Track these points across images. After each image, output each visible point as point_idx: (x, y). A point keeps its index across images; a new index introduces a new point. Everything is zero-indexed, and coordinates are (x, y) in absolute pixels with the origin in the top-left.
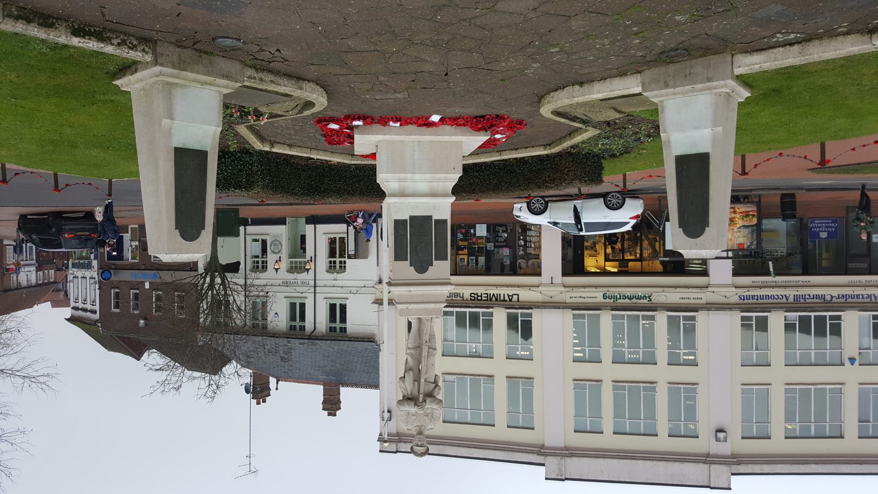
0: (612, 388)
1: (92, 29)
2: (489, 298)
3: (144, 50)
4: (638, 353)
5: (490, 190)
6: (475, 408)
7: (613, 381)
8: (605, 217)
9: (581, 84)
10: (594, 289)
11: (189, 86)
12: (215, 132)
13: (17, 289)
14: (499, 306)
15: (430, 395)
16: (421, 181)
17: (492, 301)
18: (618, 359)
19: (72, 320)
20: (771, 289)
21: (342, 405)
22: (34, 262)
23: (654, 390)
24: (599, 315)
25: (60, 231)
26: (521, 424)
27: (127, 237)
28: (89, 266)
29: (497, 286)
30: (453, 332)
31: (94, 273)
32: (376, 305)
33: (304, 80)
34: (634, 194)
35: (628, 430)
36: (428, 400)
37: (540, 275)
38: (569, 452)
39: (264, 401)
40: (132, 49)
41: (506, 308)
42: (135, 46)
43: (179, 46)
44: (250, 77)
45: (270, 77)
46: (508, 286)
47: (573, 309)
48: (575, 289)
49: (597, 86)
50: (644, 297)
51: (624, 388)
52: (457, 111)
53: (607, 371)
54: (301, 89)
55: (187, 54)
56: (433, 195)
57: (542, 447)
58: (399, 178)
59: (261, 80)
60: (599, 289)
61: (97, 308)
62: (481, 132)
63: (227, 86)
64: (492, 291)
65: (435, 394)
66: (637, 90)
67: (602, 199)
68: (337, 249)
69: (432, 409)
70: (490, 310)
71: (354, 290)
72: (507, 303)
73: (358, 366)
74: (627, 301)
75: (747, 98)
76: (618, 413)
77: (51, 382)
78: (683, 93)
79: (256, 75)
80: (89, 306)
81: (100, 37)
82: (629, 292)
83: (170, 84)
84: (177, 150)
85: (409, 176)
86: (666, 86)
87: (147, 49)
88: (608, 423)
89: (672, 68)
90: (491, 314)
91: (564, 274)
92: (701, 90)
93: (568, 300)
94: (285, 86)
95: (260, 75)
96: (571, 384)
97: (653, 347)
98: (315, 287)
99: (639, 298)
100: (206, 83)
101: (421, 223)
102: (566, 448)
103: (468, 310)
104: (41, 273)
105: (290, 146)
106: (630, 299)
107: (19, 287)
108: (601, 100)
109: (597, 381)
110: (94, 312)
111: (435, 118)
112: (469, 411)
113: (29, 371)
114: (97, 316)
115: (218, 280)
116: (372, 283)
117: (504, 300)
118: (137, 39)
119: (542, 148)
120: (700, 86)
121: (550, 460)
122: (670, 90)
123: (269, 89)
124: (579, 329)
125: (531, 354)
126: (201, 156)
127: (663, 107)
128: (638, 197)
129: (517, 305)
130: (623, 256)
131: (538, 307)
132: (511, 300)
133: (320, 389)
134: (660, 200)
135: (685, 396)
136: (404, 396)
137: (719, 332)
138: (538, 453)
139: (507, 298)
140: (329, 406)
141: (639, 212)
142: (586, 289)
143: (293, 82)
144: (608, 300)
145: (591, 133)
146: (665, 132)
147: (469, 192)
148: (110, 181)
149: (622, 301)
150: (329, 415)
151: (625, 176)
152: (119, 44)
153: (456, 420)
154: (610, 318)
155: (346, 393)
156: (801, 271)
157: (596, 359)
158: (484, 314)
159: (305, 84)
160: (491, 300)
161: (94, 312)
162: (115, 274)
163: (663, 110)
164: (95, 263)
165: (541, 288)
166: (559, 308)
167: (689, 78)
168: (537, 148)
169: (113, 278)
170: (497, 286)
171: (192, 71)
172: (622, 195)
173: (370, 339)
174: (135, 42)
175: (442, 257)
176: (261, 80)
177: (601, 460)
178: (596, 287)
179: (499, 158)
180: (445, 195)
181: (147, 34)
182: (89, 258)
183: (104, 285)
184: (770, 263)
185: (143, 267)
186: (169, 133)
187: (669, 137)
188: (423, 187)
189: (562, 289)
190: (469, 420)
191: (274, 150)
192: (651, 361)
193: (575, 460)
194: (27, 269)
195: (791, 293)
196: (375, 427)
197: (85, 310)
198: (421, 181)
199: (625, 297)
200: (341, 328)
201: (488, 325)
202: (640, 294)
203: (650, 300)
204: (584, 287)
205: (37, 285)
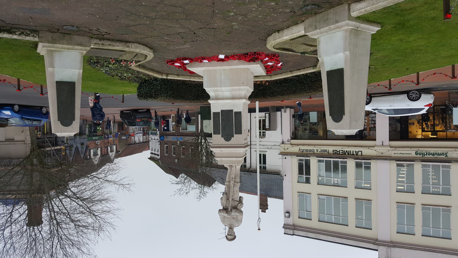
0: (421, 209)
1: (5, 29)
2: (344, 153)
3: (33, 36)
4: (439, 188)
5: (291, 93)
6: (337, 215)
7: (422, 205)
8: (408, 105)
9: (278, 31)
10: (409, 149)
11: (63, 51)
12: (79, 73)
13: (134, 144)
14: (350, 158)
15: (235, 208)
16: (226, 91)
17: (346, 155)
18: (425, 192)
19: (151, 158)
21: (269, 207)
22: (142, 132)
23: (449, 211)
24: (413, 164)
25: (135, 118)
26: (364, 226)
27: (170, 120)
28: (156, 134)
29: (349, 146)
30: (323, 172)
31: (157, 137)
32: (281, 156)
33: (130, 42)
34: (427, 91)
35: (431, 234)
36: (233, 210)
37: (375, 140)
40: (27, 36)
41: (355, 159)
42: (29, 34)
43: (52, 32)
44: (96, 44)
45: (109, 42)
46: (355, 146)
47: (396, 161)
48: (397, 149)
49: (286, 32)
50: (443, 154)
51: (429, 209)
52: (230, 52)
53: (418, 198)
54: (128, 47)
55: (56, 35)
57: (377, 240)
58: (214, 90)
59: (103, 44)
60: (412, 149)
61: (159, 153)
62: (251, 63)
63: (84, 51)
64: (346, 149)
65: (238, 207)
66: (302, 33)
67: (406, 95)
68: (263, 126)
69: (237, 216)
70: (345, 160)
71: (270, 147)
72: (355, 156)
73: (275, 187)
74: (431, 156)
75: (378, 31)
76: (425, 223)
77: (132, 188)
78: (325, 32)
79: (99, 42)
80: (156, 153)
81: (9, 32)
82: (432, 151)
83: (52, 51)
84: (57, 82)
85: (219, 88)
86: (316, 28)
87: (35, 35)
88: (418, 229)
89: (318, 17)
90: (346, 162)
91: (391, 140)
92: (334, 29)
93: (393, 155)
94: (118, 46)
95: (102, 42)
96: (395, 205)
97: (449, 185)
98: (251, 145)
99: (439, 154)
100: (69, 49)
101: (227, 114)
102: (391, 242)
103: (332, 159)
104: (145, 137)
105: (178, 75)
106: (433, 155)
107: (135, 143)
108: (291, 40)
109: (412, 204)
110: (158, 155)
111: (222, 56)
112: (333, 216)
113: (121, 182)
114: (159, 157)
115: (203, 141)
116: (279, 144)
117: (353, 154)
118: (30, 31)
119: (312, 68)
120: (332, 26)
121: (381, 248)
122: (318, 31)
123: (110, 48)
125: (371, 186)
126: (71, 86)
127: (319, 41)
128: (430, 93)
129: (360, 157)
130: (434, 129)
131: (374, 159)
132: (357, 155)
134: (449, 94)
136: (223, 208)
138: (374, 243)
139: (355, 153)
140: (262, 207)
141: (431, 102)
142: (404, 149)
143: (123, 44)
144: (418, 156)
146: (320, 57)
147: (282, 95)
148: (123, 95)
149: (428, 156)
151: (390, 81)
152: (20, 34)
153: (326, 220)
154: (421, 166)
155: (271, 201)
158: (341, 162)
159: (130, 45)
160: (345, 154)
161: (158, 155)
162: (166, 138)
163: (319, 43)
164: (158, 132)
165: (375, 148)
166: (387, 160)
167: (326, 22)
168: (310, 68)
169: (165, 140)
170: (349, 146)
171: (59, 44)
172: (419, 92)
173: (278, 173)
174: (29, 33)
176: (103, 44)
177: (414, 251)
178: (411, 147)
179: (291, 75)
181: (34, 28)
182: (156, 130)
183: (162, 142)
185: (177, 134)
186: (53, 74)
187: (323, 60)
188: (227, 94)
189: (389, 148)
190: (333, 221)
193: (398, 249)
194: (139, 135)
195: (320, 149)
196: (281, 220)
197: (155, 154)
198: (226, 91)
199: (430, 154)
200: (263, 167)
201: (344, 169)
202: (440, 152)
203: (447, 156)
204: (403, 147)
205: (143, 142)
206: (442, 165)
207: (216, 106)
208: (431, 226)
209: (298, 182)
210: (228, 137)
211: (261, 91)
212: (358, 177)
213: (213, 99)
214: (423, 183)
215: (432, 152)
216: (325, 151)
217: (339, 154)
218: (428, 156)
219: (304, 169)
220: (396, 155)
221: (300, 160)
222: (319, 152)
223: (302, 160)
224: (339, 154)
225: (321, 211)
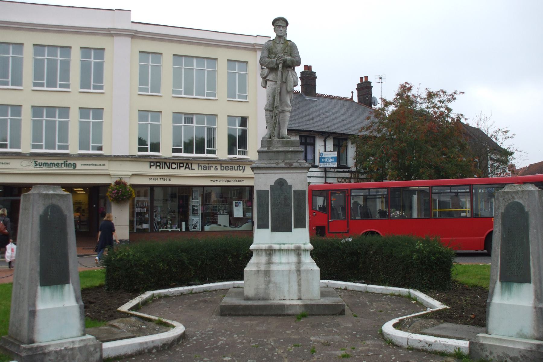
6: (189, 72)
20: (189, 175)
35: (184, 59)
38: (110, 33)
39: (361, 78)
56: (270, 252)
74: (56, 162)
101: (282, 225)
103: (194, 155)
124: (98, 137)
131: (132, 157)
133: (319, 90)
135: (148, 81)
136: (294, 69)
137: (120, 138)
144: (72, 162)
145: (125, 308)
149: (60, 162)
150: (310, 67)
156: (155, 189)
157: (84, 111)
175: (263, 194)
179: (194, 287)
180: (258, 250)
184: (415, 197)
191: (407, 290)
192: (37, 110)
195: (212, 172)
197: (497, 161)
201: (176, 142)
202: (44, 168)
203: (35, 162)
206: (42, 148)
207: (301, 237)
208: (206, 71)
209: (216, 115)
210: (281, 183)
211: (231, 260)
212: (156, 129)
213: (306, 250)
214: (214, 129)
215: (54, 168)
216: (205, 168)
217: (180, 163)
218: (60, 162)
219: (238, 142)
220: (102, 163)
221: (244, 153)
222: (214, 166)
223: (209, 152)
224: (151, 162)
225: (212, 76)
